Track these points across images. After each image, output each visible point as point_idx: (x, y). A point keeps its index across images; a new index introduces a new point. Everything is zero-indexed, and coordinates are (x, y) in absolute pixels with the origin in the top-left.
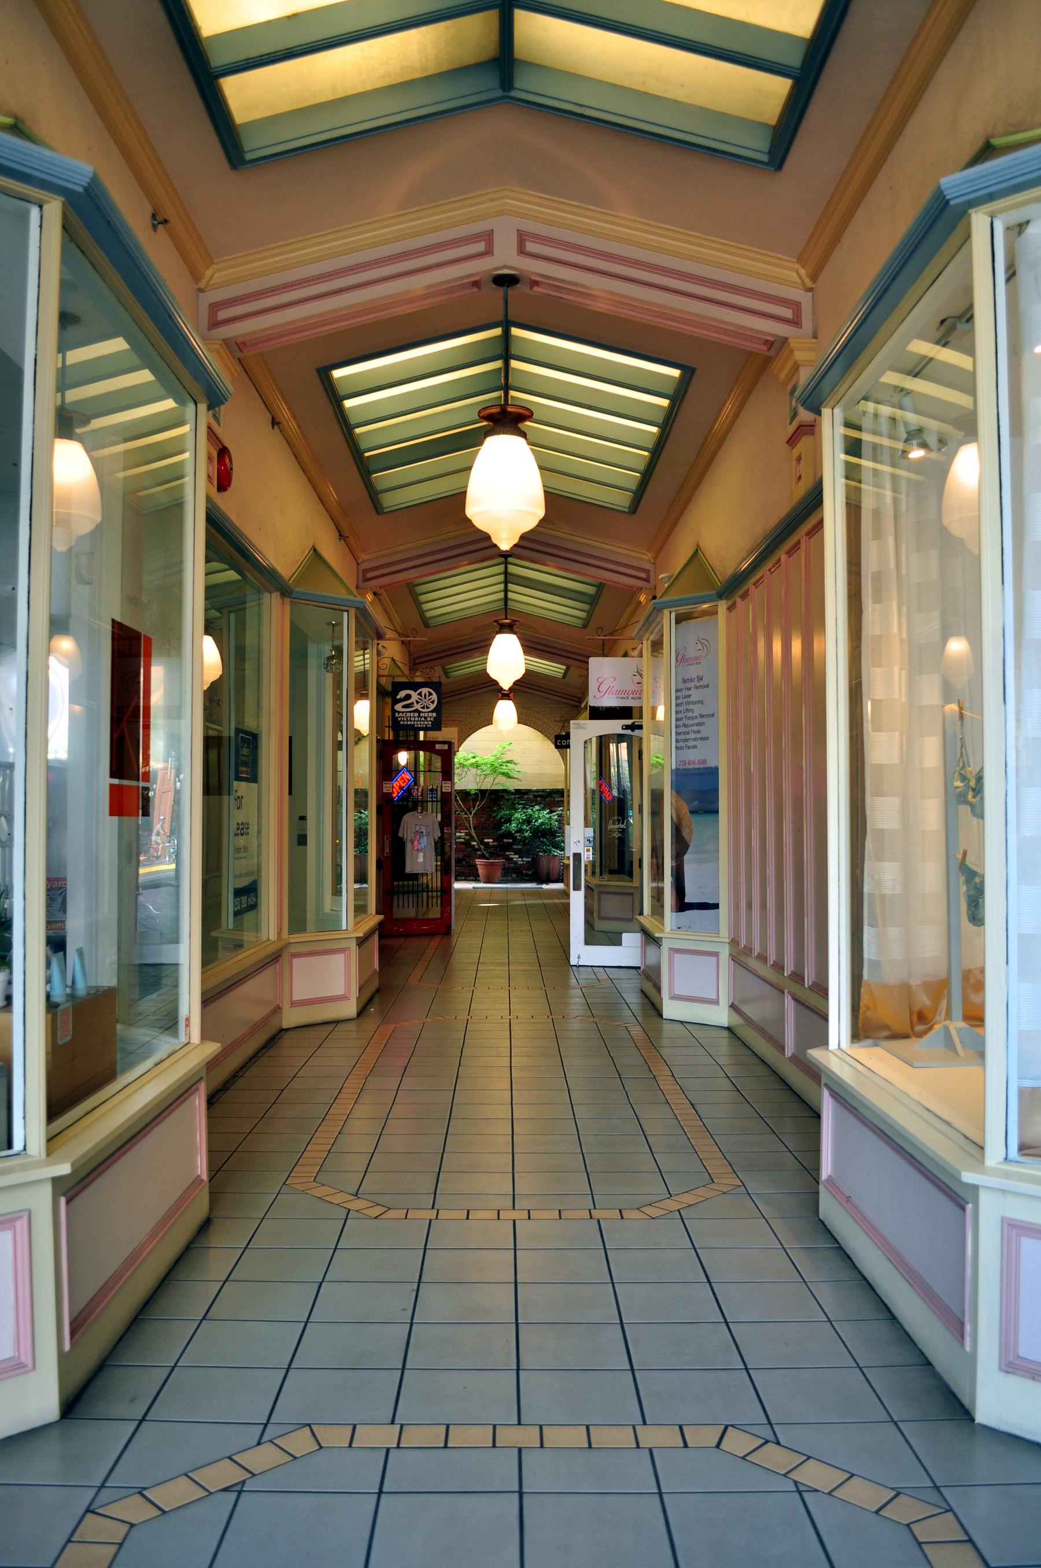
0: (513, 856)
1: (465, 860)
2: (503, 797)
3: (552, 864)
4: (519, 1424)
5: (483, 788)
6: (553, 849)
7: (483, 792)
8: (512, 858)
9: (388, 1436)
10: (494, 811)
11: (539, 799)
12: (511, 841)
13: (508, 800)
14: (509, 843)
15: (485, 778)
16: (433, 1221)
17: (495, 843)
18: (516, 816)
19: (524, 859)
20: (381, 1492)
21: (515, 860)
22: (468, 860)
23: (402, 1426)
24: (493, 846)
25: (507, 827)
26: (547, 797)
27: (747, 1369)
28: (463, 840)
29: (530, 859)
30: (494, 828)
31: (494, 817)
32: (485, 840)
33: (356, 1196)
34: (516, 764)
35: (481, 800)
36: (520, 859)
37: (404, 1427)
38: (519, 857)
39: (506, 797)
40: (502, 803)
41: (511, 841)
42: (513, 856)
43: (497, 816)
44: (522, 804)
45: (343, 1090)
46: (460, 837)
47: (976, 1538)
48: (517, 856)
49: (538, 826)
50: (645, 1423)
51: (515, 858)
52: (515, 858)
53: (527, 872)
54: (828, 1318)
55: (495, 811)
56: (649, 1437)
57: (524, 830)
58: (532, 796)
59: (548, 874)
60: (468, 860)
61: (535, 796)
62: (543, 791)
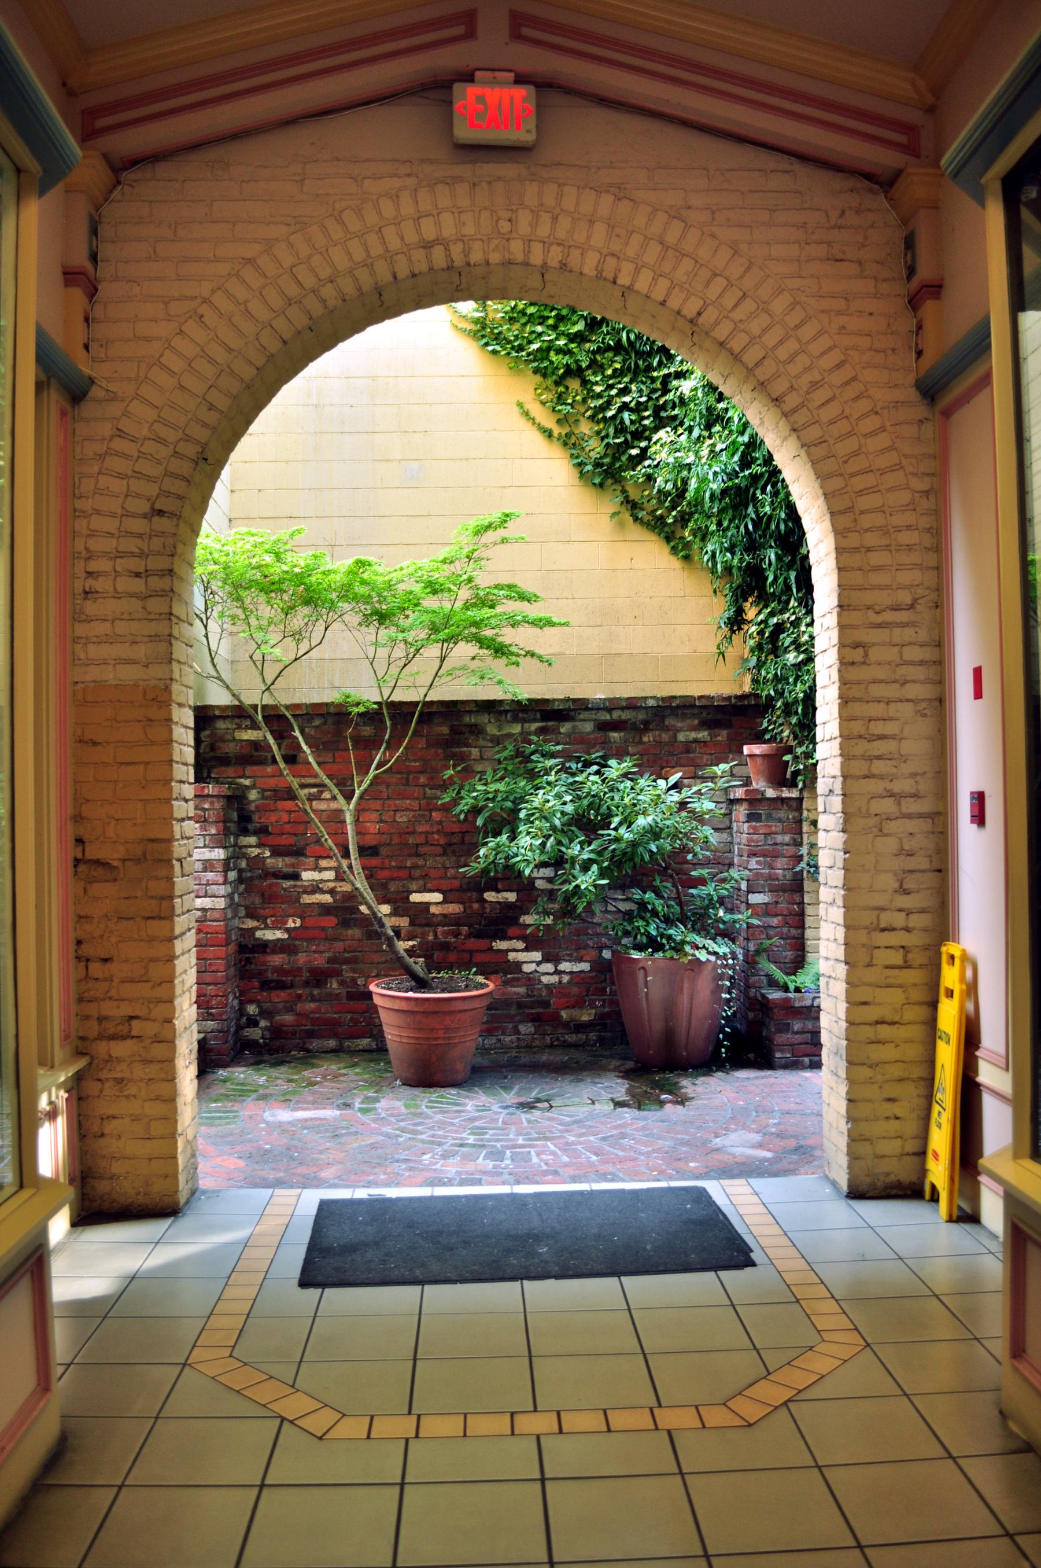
0: (522, 956)
1: (337, 973)
2: (477, 730)
3: (685, 998)
4: (535, 1410)
5: (398, 697)
6: (692, 937)
7: (401, 711)
8: (518, 965)
9: (406, 1426)
10: (444, 786)
11: (615, 735)
12: (512, 897)
13: (497, 741)
14: (507, 906)
15: (174, 299)
16: (411, 1441)
17: (454, 908)
18: (537, 801)
19: (565, 966)
20: (402, 1485)
21: (527, 968)
22: (348, 975)
23: (419, 1416)
24: (446, 919)
25: (497, 849)
26: (646, 726)
27: (733, 1305)
28: (327, 898)
29: (585, 966)
30: (447, 849)
31: (447, 808)
32: (415, 898)
33: (293, 1386)
34: (520, 405)
35: (392, 746)
36: (549, 967)
37: (422, 1417)
38: (546, 959)
39: (492, 730)
40: (475, 752)
41: (512, 897)
42: (522, 956)
43: (455, 802)
44: (553, 755)
45: (214, 1322)
46: (315, 888)
47: (859, 1328)
48: (537, 956)
49: (634, 844)
50: (660, 1406)
51: (530, 960)
52: (530, 960)
53: (575, 1013)
54: (902, 1389)
55: (451, 780)
56: (667, 1418)
57: (573, 860)
58: (588, 727)
59: (669, 1036)
60: (348, 975)
61: (604, 727)
62: (632, 704)
